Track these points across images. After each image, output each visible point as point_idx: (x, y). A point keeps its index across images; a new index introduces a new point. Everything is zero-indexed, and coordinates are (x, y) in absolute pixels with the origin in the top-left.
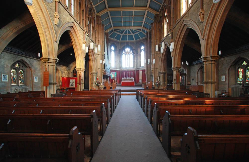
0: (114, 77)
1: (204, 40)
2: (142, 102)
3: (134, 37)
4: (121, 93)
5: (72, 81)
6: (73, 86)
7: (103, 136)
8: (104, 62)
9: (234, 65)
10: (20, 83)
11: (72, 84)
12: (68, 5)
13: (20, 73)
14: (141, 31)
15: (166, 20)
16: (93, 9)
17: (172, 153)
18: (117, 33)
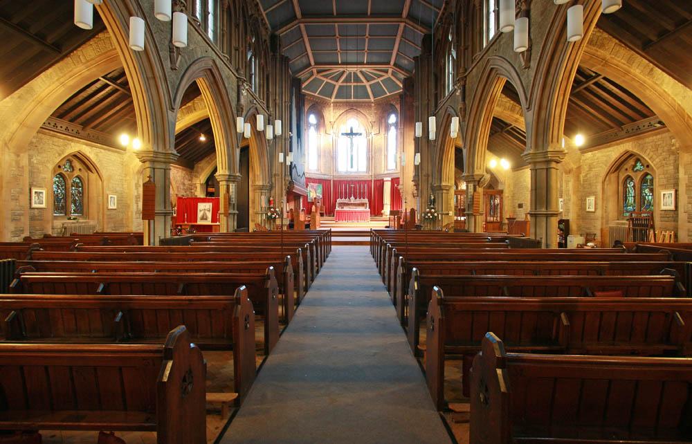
0: (315, 198)
1: (531, 112)
2: (384, 267)
3: (369, 90)
4: (334, 239)
5: (204, 208)
6: (206, 219)
7: (288, 324)
8: (289, 159)
9: (616, 171)
10: (73, 212)
11: (204, 214)
12: (201, 15)
13: (72, 186)
14: (389, 75)
15: (450, 54)
16: (263, 20)
17: (418, 346)
18: (325, 79)
